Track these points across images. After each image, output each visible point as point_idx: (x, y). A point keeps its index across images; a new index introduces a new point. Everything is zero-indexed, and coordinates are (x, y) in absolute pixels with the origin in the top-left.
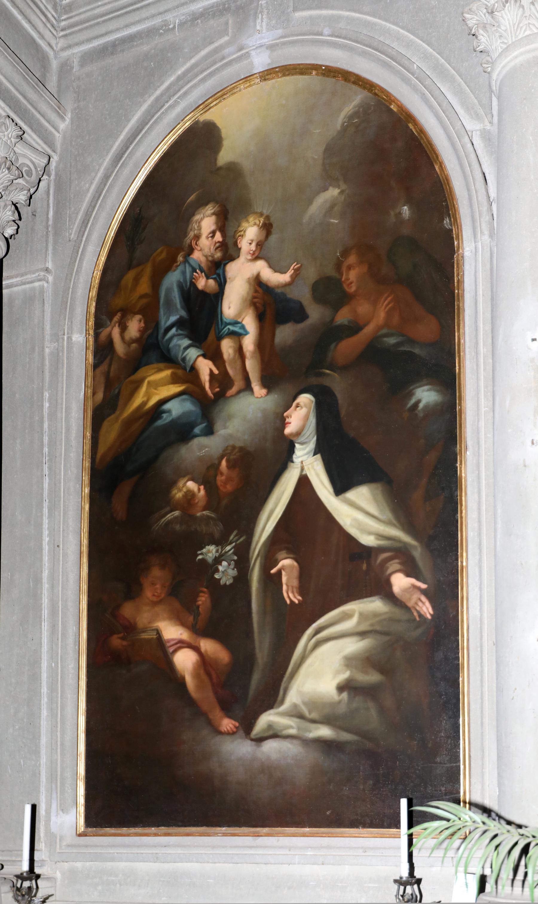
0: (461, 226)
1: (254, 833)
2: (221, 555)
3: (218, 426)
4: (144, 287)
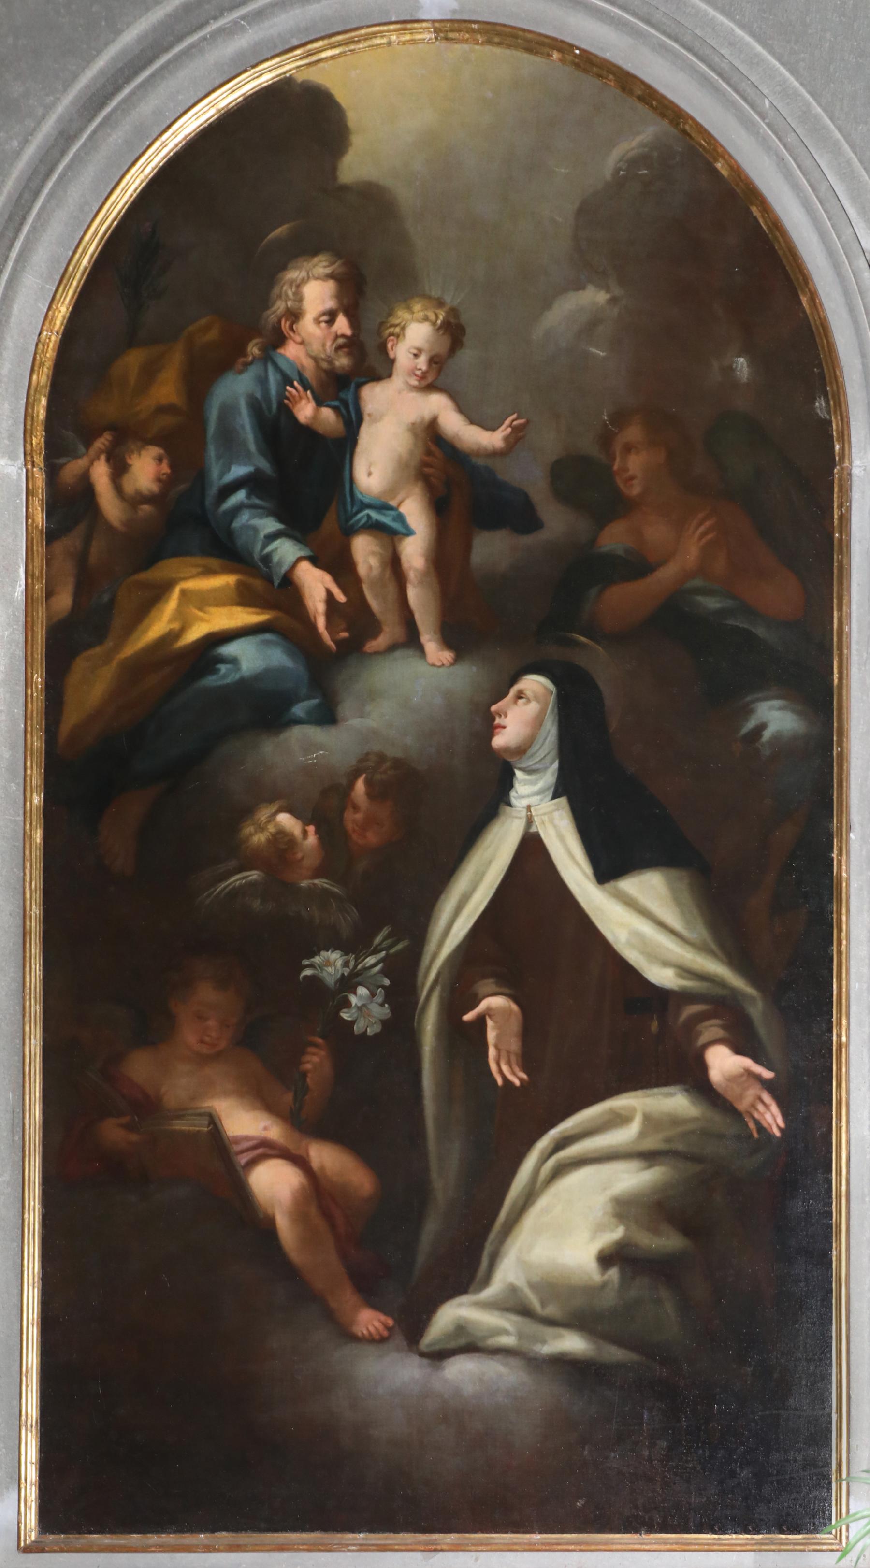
0: (848, 418)
1: (427, 1543)
2: (354, 974)
3: (346, 708)
4: (167, 390)
